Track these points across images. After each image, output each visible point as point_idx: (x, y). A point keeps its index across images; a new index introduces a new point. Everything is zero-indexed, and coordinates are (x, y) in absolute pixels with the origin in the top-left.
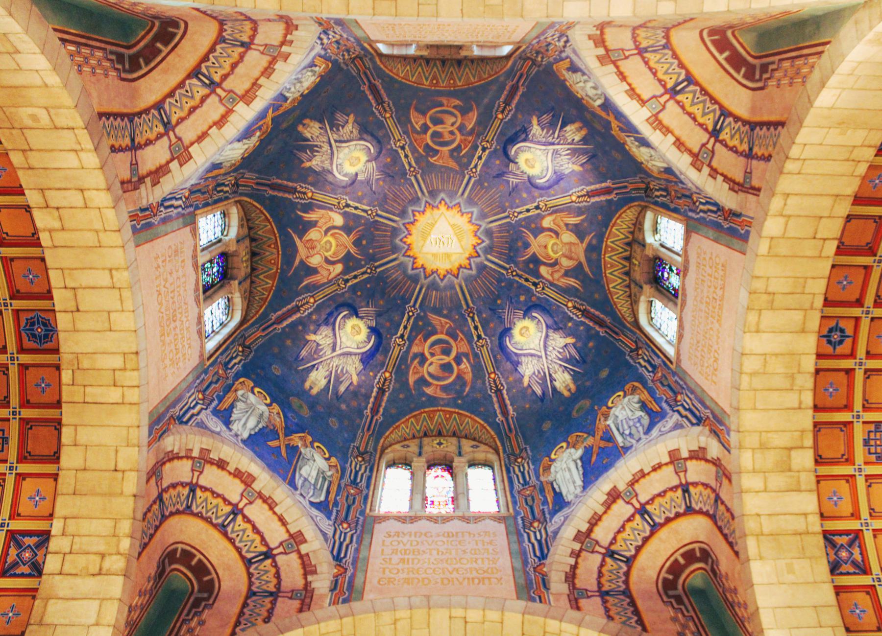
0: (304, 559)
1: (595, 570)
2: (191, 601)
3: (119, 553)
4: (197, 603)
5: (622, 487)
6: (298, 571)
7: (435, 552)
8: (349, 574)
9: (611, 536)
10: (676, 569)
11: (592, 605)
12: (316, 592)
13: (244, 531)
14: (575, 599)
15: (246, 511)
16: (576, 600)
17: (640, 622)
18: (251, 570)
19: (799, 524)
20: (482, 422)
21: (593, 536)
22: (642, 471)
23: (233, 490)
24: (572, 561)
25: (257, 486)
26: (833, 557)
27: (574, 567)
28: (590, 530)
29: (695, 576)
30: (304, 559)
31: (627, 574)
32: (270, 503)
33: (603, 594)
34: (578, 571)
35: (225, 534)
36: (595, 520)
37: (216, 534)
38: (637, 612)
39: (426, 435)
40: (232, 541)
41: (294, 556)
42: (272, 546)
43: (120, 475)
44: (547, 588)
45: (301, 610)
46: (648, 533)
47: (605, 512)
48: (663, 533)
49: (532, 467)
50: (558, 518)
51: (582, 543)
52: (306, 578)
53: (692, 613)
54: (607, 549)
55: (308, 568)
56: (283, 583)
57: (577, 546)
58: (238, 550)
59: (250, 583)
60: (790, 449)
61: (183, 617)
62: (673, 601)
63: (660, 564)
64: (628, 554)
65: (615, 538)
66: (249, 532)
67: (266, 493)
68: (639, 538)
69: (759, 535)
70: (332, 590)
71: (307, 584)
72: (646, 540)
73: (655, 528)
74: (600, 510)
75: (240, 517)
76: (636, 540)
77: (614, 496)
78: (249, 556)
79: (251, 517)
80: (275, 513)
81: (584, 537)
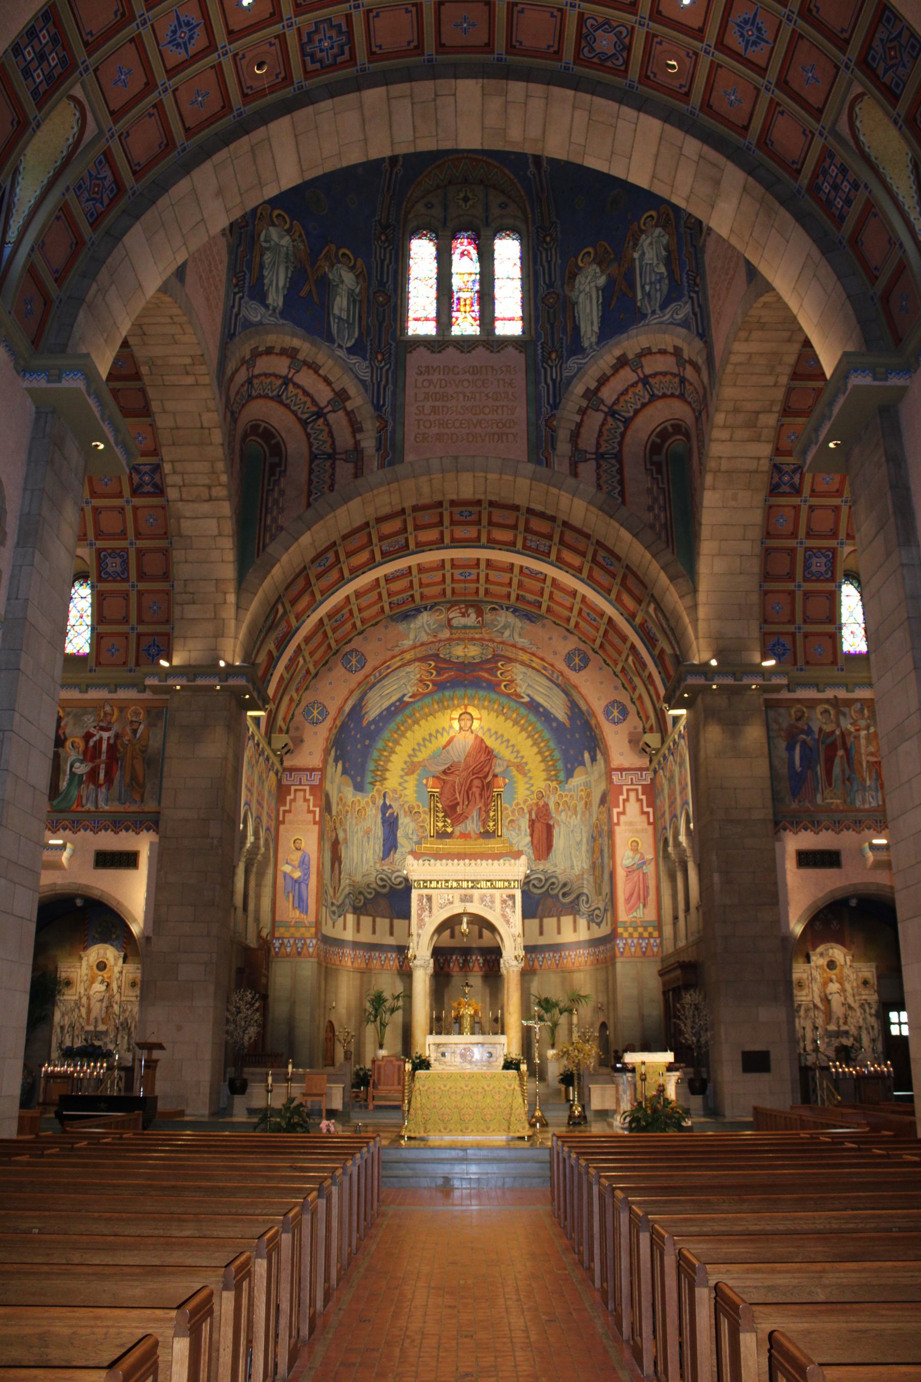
0: (350, 414)
1: (597, 428)
2: (267, 468)
3: (220, 485)
4: (273, 467)
5: (630, 356)
6: (347, 431)
7: (461, 397)
8: (390, 428)
9: (615, 397)
10: (663, 435)
11: (587, 469)
12: (365, 453)
13: (296, 395)
14: (577, 458)
15: (296, 379)
16: (576, 463)
17: (622, 493)
18: (309, 430)
19: (753, 465)
20: (512, 177)
21: (600, 394)
22: (649, 348)
23: (281, 366)
24: (578, 418)
25: (301, 356)
26: (776, 479)
27: (579, 425)
28: (598, 389)
29: (676, 443)
30: (350, 414)
31: (623, 435)
32: (314, 367)
33: (600, 457)
34: (582, 430)
35: (281, 402)
36: (603, 381)
37: (273, 405)
38: (621, 482)
39: (450, 183)
40: (287, 407)
41: (341, 413)
42: (322, 405)
43: (207, 431)
44: (554, 449)
45: (356, 476)
46: (646, 400)
47: (613, 375)
48: (659, 404)
49: (559, 261)
50: (572, 363)
51: (589, 401)
52: (354, 437)
53: (665, 486)
54: (610, 408)
55: (356, 428)
56: (337, 443)
57: (584, 403)
58: (294, 413)
59: (310, 445)
60: (758, 413)
61: (266, 488)
62: (654, 468)
63: (652, 428)
64: (626, 415)
65: (618, 399)
66: (301, 396)
67: (309, 360)
68: (639, 403)
69: (716, 472)
70: (378, 450)
71: (357, 443)
72: (644, 406)
73: (653, 398)
74: (609, 372)
75: (291, 387)
76: (635, 404)
77: (622, 362)
78: (305, 416)
79: (300, 383)
80: (320, 375)
81: (591, 394)
